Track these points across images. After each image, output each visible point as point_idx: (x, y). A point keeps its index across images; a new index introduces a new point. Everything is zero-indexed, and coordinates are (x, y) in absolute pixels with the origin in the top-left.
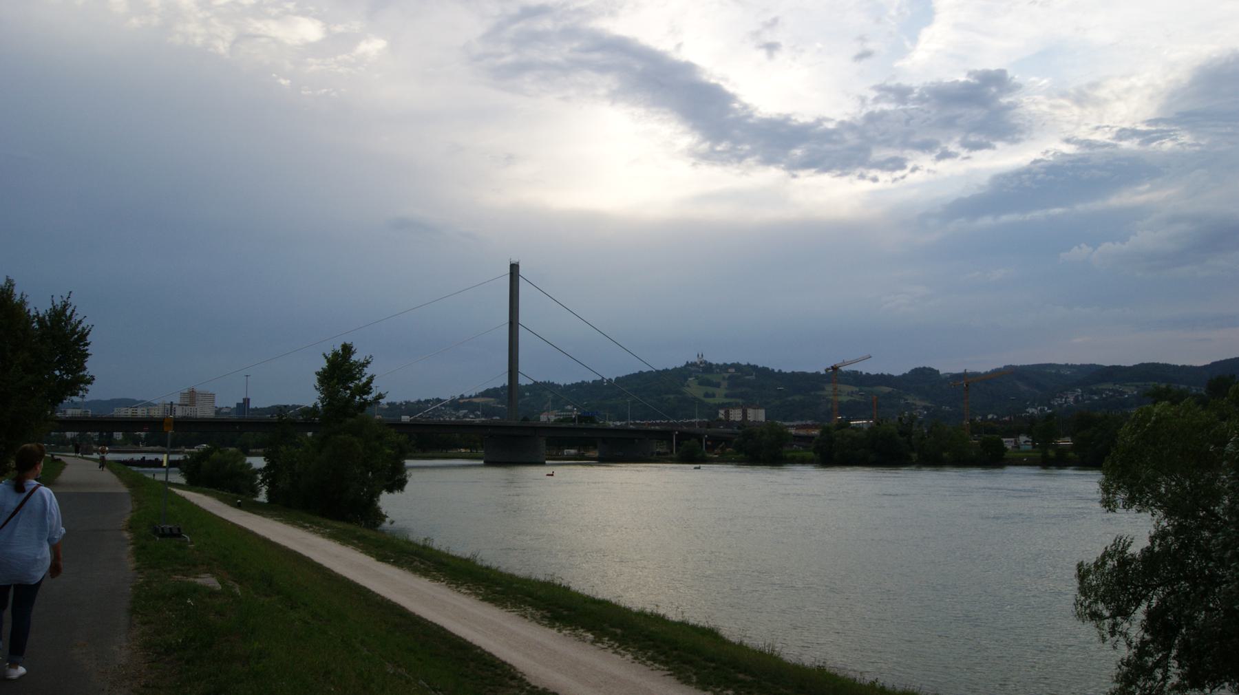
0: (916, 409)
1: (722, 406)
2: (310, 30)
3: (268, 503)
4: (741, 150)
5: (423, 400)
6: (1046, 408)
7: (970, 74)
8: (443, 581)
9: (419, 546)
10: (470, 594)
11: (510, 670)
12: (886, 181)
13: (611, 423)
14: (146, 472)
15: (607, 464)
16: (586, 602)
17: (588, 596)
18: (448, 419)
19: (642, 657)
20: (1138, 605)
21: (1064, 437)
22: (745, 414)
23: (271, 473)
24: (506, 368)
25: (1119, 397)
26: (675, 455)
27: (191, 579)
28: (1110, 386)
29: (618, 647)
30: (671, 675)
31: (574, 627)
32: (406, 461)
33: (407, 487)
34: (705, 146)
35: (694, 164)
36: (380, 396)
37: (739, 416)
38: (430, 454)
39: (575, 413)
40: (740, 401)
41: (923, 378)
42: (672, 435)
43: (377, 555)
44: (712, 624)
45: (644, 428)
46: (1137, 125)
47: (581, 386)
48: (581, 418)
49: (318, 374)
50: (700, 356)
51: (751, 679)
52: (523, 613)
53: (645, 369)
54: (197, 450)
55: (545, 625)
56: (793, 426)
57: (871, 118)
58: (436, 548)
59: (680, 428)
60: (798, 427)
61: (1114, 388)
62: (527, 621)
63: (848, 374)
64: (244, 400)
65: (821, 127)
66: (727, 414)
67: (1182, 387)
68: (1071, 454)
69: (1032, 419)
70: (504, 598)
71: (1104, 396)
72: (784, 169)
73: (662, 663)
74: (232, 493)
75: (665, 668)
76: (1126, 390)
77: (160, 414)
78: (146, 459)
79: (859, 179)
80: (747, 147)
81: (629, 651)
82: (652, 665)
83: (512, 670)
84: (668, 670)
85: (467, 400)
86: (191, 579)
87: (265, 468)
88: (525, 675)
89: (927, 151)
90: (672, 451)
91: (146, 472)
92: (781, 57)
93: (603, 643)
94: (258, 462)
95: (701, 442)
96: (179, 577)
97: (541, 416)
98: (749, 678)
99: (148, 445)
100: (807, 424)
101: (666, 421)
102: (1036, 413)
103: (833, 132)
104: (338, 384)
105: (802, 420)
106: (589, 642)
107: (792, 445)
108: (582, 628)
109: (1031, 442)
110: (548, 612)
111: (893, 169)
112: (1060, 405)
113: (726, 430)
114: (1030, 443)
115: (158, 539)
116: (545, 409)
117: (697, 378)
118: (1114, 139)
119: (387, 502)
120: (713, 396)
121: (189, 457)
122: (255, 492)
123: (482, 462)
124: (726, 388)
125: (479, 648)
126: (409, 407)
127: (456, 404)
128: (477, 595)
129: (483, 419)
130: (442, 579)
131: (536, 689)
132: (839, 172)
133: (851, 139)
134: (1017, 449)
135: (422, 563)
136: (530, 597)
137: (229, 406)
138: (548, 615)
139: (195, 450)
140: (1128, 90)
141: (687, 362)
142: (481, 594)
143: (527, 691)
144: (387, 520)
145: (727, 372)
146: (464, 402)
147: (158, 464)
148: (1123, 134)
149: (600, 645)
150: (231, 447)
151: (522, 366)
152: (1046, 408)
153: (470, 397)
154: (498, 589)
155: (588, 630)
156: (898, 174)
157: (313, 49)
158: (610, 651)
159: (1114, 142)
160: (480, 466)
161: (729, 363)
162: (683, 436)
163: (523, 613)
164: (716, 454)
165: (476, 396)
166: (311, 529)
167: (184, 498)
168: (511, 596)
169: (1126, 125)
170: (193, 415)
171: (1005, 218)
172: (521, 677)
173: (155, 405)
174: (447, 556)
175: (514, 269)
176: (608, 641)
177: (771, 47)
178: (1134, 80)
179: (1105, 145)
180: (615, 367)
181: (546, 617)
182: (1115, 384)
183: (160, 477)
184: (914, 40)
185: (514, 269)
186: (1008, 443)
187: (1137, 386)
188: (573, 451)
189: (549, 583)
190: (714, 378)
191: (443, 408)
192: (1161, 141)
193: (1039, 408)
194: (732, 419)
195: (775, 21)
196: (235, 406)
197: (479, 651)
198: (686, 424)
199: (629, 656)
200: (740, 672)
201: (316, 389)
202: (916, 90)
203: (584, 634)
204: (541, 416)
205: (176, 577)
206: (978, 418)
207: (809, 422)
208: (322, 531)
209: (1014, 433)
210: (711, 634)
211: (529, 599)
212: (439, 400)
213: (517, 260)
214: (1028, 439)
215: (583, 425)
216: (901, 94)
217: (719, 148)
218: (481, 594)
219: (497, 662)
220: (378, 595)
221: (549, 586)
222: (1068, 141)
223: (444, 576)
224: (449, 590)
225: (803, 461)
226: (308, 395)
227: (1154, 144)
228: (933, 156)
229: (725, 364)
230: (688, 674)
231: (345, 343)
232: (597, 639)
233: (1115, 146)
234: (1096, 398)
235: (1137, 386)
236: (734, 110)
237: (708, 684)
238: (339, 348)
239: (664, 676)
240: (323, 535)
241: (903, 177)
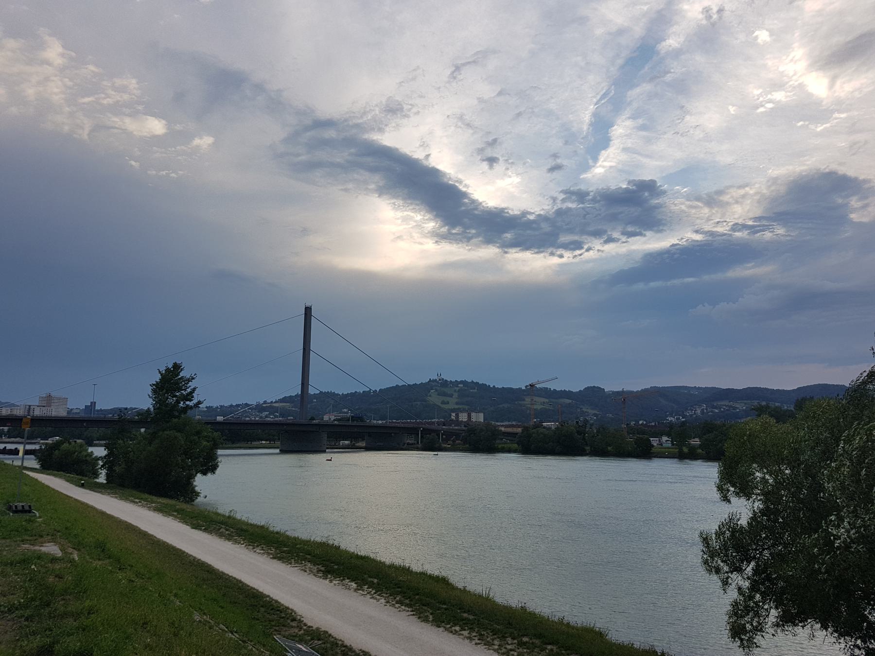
0: (589, 415)
1: (453, 410)
2: (156, 126)
3: (107, 483)
4: (469, 233)
5: (234, 404)
6: (681, 418)
7: (629, 182)
8: (243, 544)
9: (225, 516)
10: (263, 553)
11: (291, 613)
12: (569, 257)
13: (375, 422)
14: (6, 459)
16: (351, 558)
17: (353, 553)
18: (253, 419)
19: (393, 601)
20: (749, 563)
21: (694, 438)
22: (469, 416)
23: (109, 462)
25: (733, 411)
26: (420, 445)
27: (37, 548)
28: (726, 403)
29: (375, 593)
30: (413, 615)
31: (342, 578)
32: (219, 450)
33: (218, 471)
34: (445, 229)
35: (437, 242)
36: (199, 403)
37: (466, 417)
38: (238, 445)
39: (349, 414)
40: (466, 407)
41: (593, 394)
43: (191, 524)
44: (444, 574)
45: (398, 425)
46: (746, 221)
47: (354, 395)
48: (353, 418)
50: (439, 375)
51: (473, 617)
52: (303, 568)
53: (401, 384)
54: (51, 442)
55: (321, 577)
56: (503, 426)
57: (559, 213)
58: (239, 518)
59: (424, 426)
60: (506, 426)
61: (729, 404)
62: (306, 574)
63: (541, 389)
64: (91, 403)
65: (526, 219)
66: (457, 415)
67: (777, 404)
68: (700, 451)
69: (671, 425)
70: (289, 556)
71: (722, 410)
72: (498, 247)
73: (407, 605)
74: (78, 475)
75: (410, 609)
76: (737, 406)
77: (21, 413)
78: (7, 448)
79: (550, 256)
80: (474, 231)
81: (383, 596)
82: (400, 607)
83: (293, 614)
84: (412, 611)
85: (269, 405)
86: (37, 548)
87: (106, 456)
88: (303, 617)
89: (598, 237)
90: (418, 443)
91: (6, 459)
92: (499, 167)
93: (363, 590)
94: (99, 452)
95: (438, 435)
96: (27, 546)
97: (325, 417)
98: (471, 617)
99: (9, 438)
100: (513, 424)
101: (414, 421)
102: (673, 420)
103: (533, 222)
105: (509, 421)
106: (352, 590)
107: (502, 439)
108: (348, 578)
109: (671, 441)
110: (323, 566)
111: (574, 249)
112: (691, 416)
113: (456, 428)
114: (670, 442)
115: (11, 514)
116: (327, 411)
117: (436, 390)
118: (729, 231)
119: (201, 482)
120: (448, 403)
121: (43, 447)
122: (96, 475)
123: (278, 451)
124: (457, 398)
125: (268, 596)
126: (223, 410)
127: (260, 408)
128: (269, 554)
129: (281, 419)
130: (242, 542)
131: (311, 629)
132: (536, 250)
133: (546, 227)
134: (660, 446)
135: (227, 530)
136: (309, 555)
137: (78, 407)
138: (323, 569)
139: (50, 441)
140: (744, 196)
142: (271, 554)
143: (304, 630)
144: (202, 495)
145: (458, 387)
146: (267, 406)
147: (16, 452)
148: (736, 227)
149: (361, 592)
150: (79, 439)
152: (681, 418)
153: (272, 402)
154: (285, 549)
155: (352, 581)
156: (578, 252)
157: (155, 140)
158: (369, 596)
159: (730, 233)
160: (277, 454)
162: (426, 431)
163: (303, 568)
164: (448, 445)
165: (276, 402)
166: (140, 504)
167: (36, 480)
168: (295, 555)
169: (740, 221)
170: (49, 414)
171: (653, 284)
172: (300, 619)
173: (18, 406)
174: (247, 524)
175: (308, 310)
176: (367, 588)
177: (492, 161)
178: (747, 189)
179: (725, 235)
180: (378, 382)
181: (321, 571)
182: (730, 402)
183: (18, 463)
184: (596, 159)
185: (308, 310)
186: (654, 441)
187: (745, 404)
188: (347, 442)
189: (324, 543)
191: (250, 411)
192: (763, 233)
193: (676, 417)
194: (461, 420)
195: (495, 141)
196: (84, 408)
197: (268, 599)
198: (428, 423)
199: (383, 601)
200: (465, 612)
202: (592, 194)
203: (349, 583)
204: (325, 417)
205: (25, 546)
206: (633, 423)
207: (514, 423)
208: (149, 506)
209: (659, 435)
210: (443, 581)
211: (309, 557)
212: (247, 405)
214: (668, 439)
215: (355, 423)
216: (581, 196)
217: (454, 231)
218: (271, 554)
219: (282, 607)
220: (191, 556)
221: (323, 545)
222: (697, 232)
223: (244, 540)
224: (247, 550)
225: (509, 451)
226: (144, 402)
227: (758, 234)
228: (602, 241)
230: (426, 614)
231: (176, 362)
232: (359, 588)
233: (730, 235)
234: (717, 411)
235: (745, 404)
236: (464, 204)
237: (441, 622)
239: (409, 615)
240: (149, 508)
241: (581, 255)
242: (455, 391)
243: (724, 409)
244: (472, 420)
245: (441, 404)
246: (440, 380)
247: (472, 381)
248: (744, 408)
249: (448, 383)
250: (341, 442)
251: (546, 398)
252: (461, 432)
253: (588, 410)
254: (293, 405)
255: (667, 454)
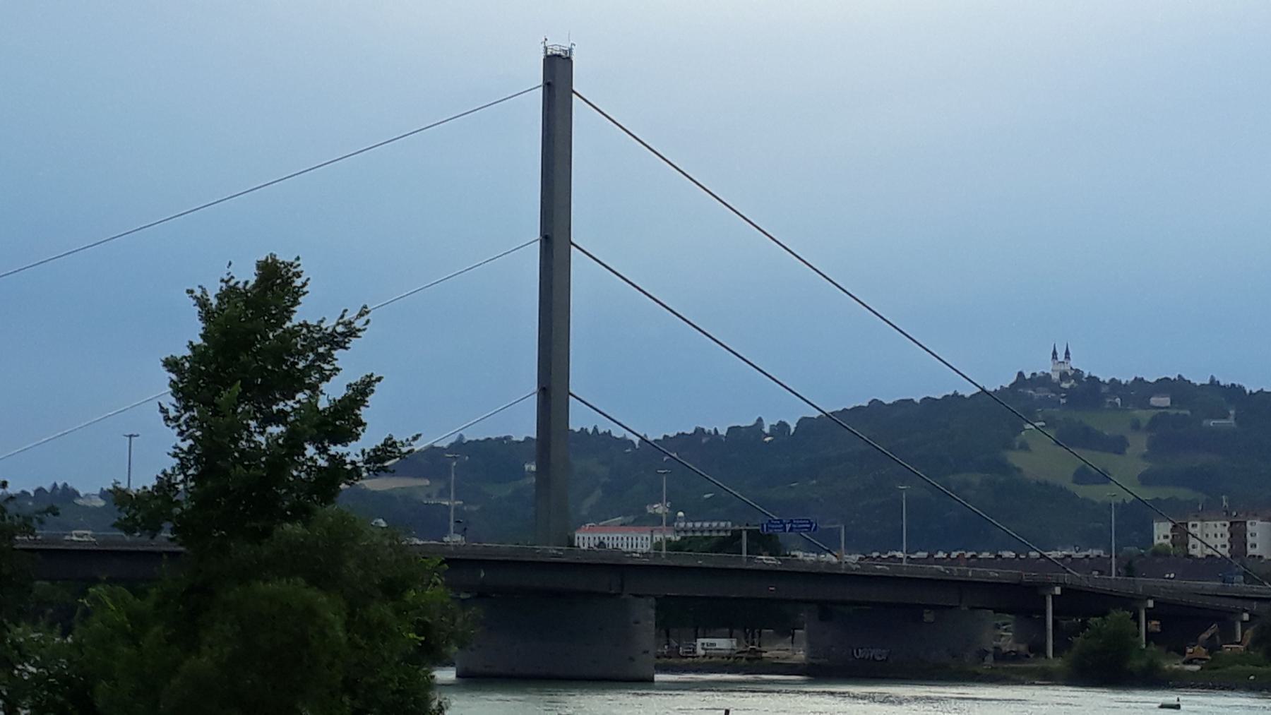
15: (940, 684)
22: (1238, 535)
24: (531, 383)
42: (1044, 598)
49: (172, 364)
50: (1061, 357)
66: (1180, 533)
104: (241, 398)
116: (584, 513)
120: (1105, 478)
124: (1144, 457)
141: (1021, 374)
151: (580, 378)
161: (1152, 379)
164: (1190, 662)
188: (723, 644)
190: (1104, 423)
201: (167, 419)
213: (567, 46)
229: (1139, 381)
238: (247, 275)
242: (1136, 426)
244: (1251, 551)
245: (1075, 482)
246: (1064, 376)
247: (1212, 380)
249: (1104, 389)
250: (700, 641)
252: (1233, 604)
255: (1252, 677)
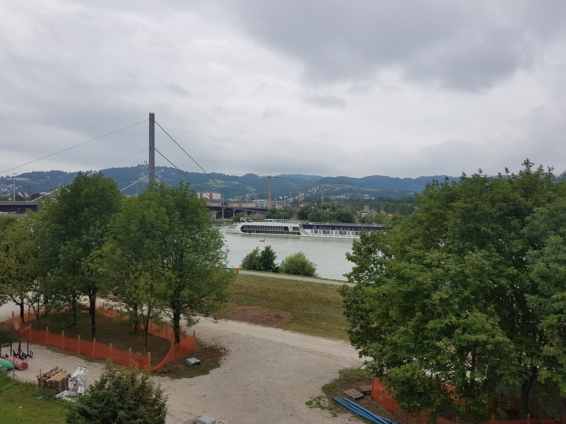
50: (146, 162)
146: (10, 180)
153: (13, 177)
165: (17, 177)
175: (152, 116)
185: (152, 116)
235: (340, 186)
243: (329, 189)
246: (146, 165)
248: (339, 189)
251: (222, 180)
253: (250, 189)
254: (31, 179)
